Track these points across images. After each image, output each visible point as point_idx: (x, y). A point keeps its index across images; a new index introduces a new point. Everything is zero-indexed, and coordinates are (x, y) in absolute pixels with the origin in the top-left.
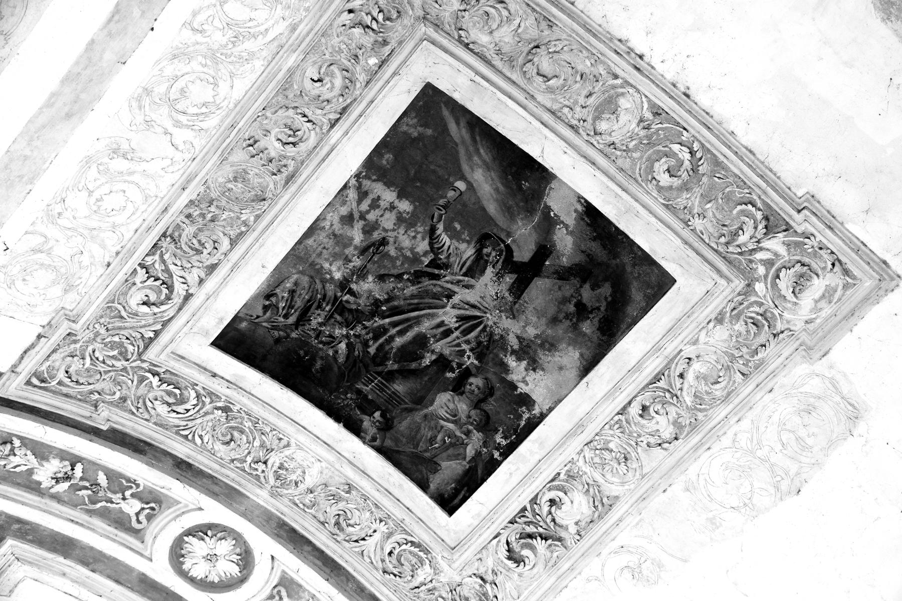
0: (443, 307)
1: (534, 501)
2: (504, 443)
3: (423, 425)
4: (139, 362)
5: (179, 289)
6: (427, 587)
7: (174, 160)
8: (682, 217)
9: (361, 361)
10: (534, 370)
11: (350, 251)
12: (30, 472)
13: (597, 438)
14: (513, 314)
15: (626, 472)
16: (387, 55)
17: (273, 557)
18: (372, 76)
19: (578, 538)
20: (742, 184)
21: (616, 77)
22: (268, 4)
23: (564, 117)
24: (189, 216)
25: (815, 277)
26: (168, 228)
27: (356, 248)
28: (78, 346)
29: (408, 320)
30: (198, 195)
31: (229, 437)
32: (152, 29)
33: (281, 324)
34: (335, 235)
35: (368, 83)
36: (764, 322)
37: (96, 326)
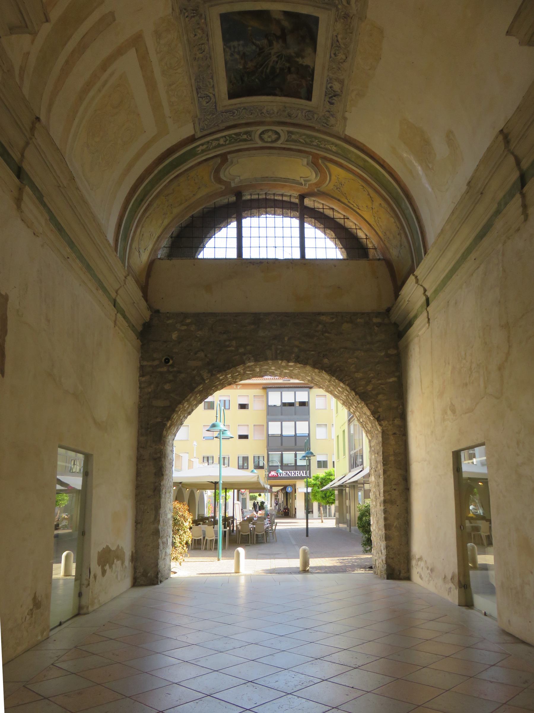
5: (211, 95)
31: (251, 113)
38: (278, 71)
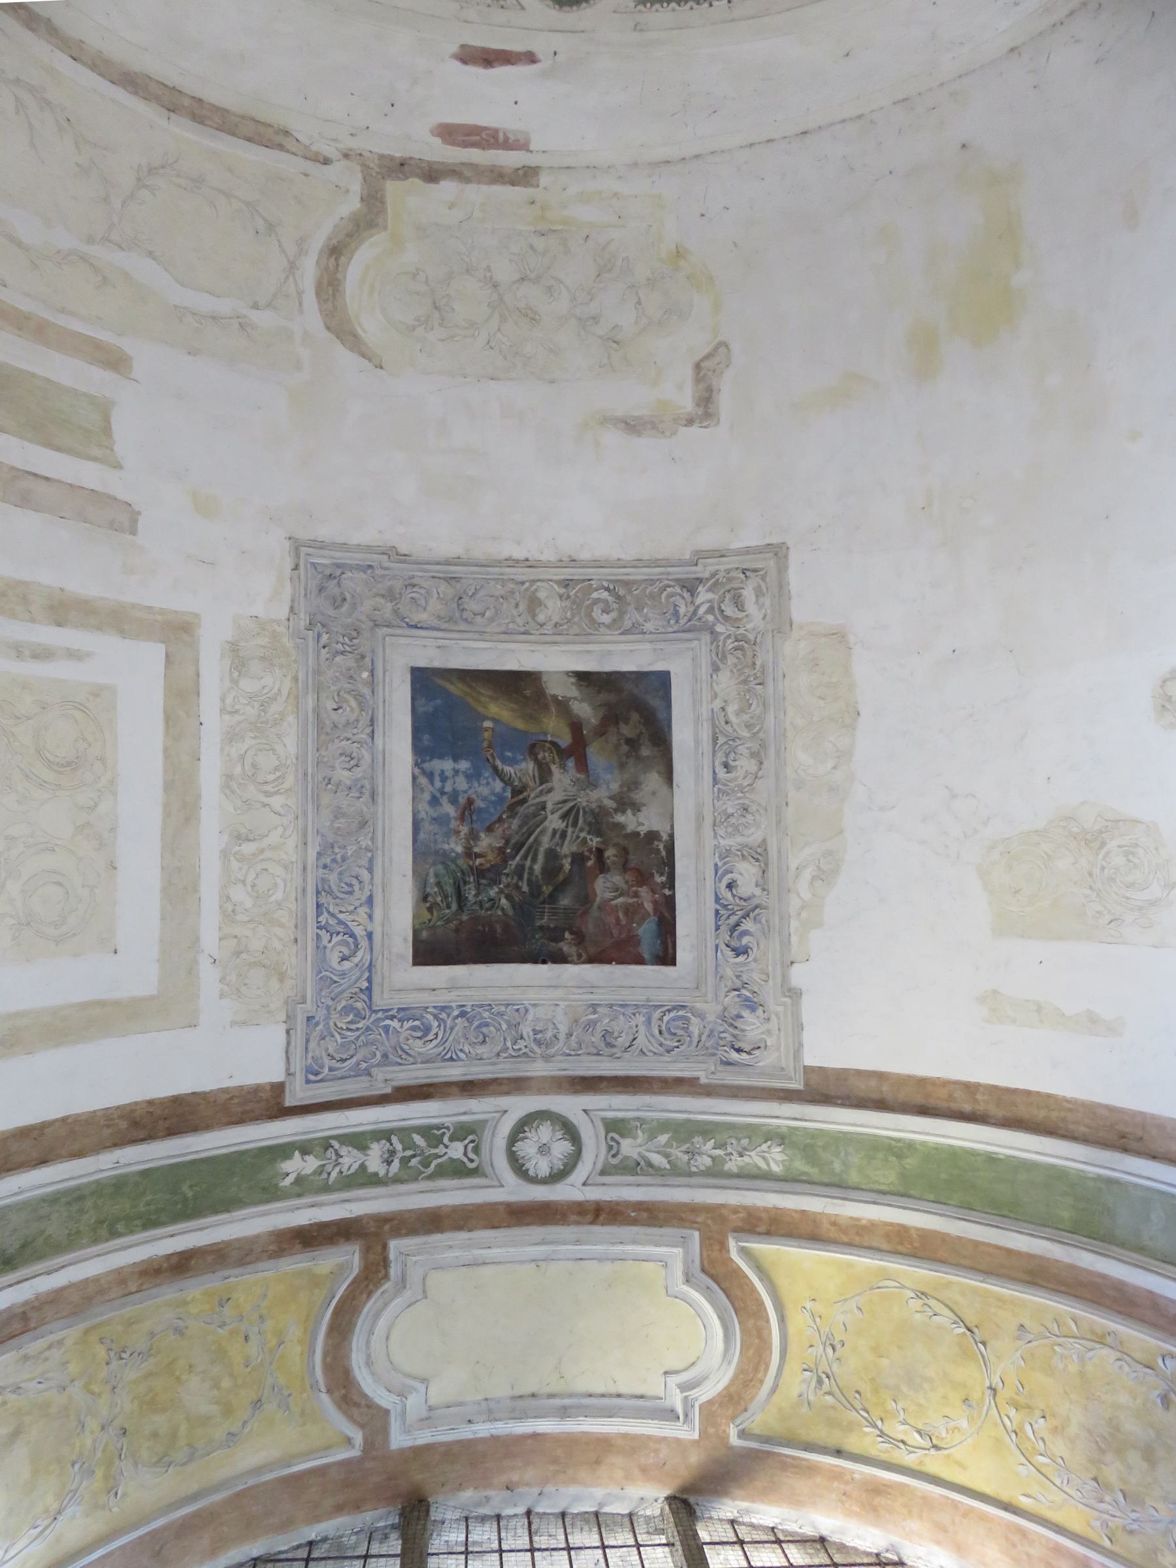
0: (546, 818)
1: (717, 899)
2: (664, 879)
4: (374, 1015)
5: (359, 931)
6: (706, 1034)
8: (637, 632)
10: (639, 810)
12: (363, 1167)
14: (594, 785)
17: (585, 1111)
18: (372, 682)
21: (523, 583)
24: (325, 867)
25: (743, 590)
26: (317, 885)
27: (456, 819)
31: (481, 1037)
32: (201, 724)
34: (434, 819)
36: (741, 643)
37: (322, 1001)
38: (567, 865)
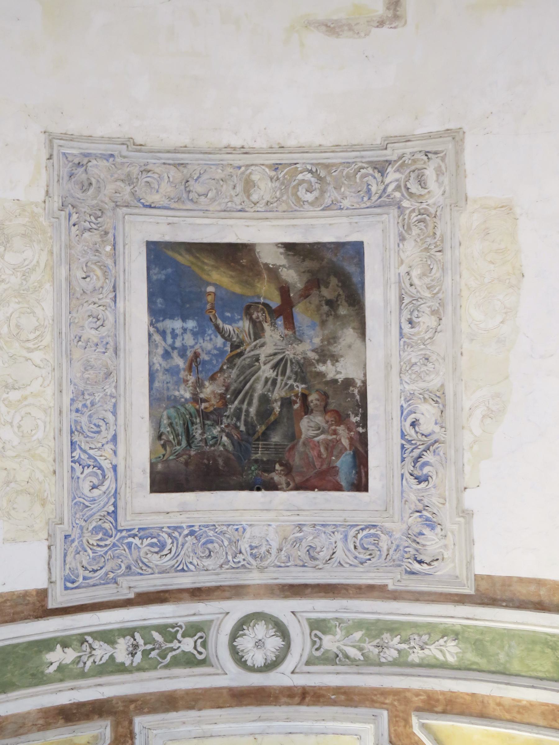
0: (259, 369)
1: (403, 435)
2: (358, 419)
3: (307, 451)
5: (106, 465)
7: (43, 376)
8: (335, 208)
9: (242, 440)
10: (337, 361)
11: (183, 374)
12: (112, 658)
13: (402, 363)
15: (433, 366)
16: (113, 240)
19: (444, 429)
20: (348, 165)
21: (239, 168)
22: (28, 245)
23: (232, 209)
24: (77, 411)
26: (71, 426)
27: (184, 370)
28: (76, 543)
29: (247, 393)
30: (73, 393)
31: (207, 552)
33: (180, 451)
34: (167, 370)
35: (115, 263)
37: (77, 522)
